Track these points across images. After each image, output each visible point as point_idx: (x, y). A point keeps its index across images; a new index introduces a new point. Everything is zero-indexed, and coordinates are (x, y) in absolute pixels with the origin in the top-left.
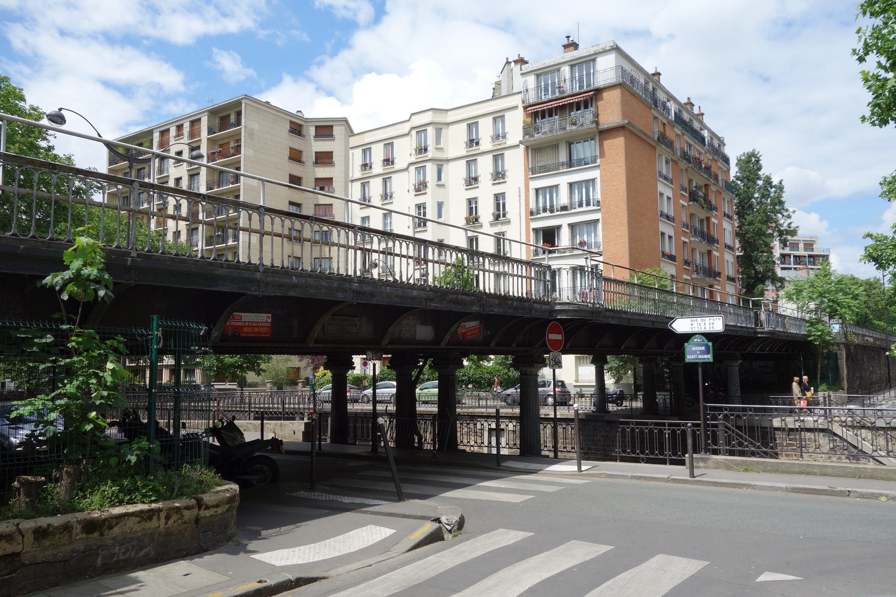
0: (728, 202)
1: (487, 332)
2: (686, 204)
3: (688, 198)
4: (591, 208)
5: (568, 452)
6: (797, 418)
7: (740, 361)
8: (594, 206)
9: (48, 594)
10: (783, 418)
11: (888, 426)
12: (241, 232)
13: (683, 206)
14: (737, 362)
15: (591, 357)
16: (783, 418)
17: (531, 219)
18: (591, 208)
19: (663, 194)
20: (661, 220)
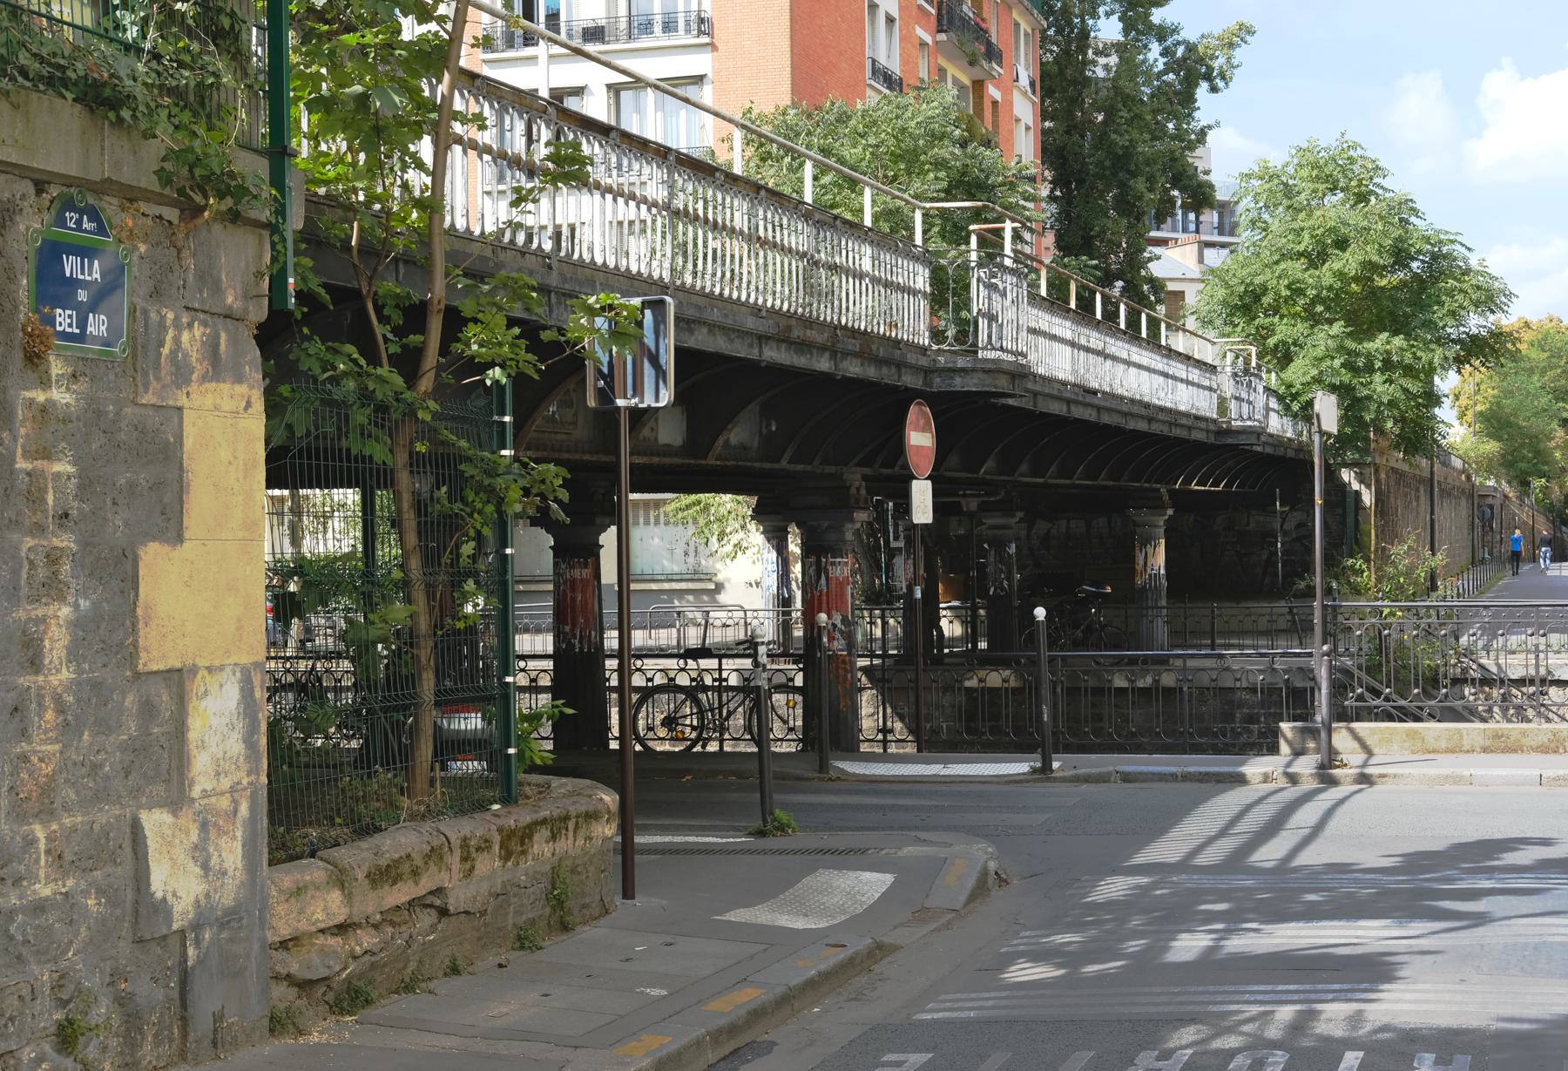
0: (1026, 34)
1: (768, 425)
2: (928, 39)
3: (933, 20)
4: (681, 38)
5: (660, 739)
6: (724, 684)
7: (1170, 512)
8: (688, 31)
9: (1246, 836)
10: (650, 684)
11: (1213, 684)
12: (458, 149)
13: (923, 44)
14: (1013, 516)
15: (754, 500)
16: (650, 684)
17: (484, 61)
18: (681, 38)
19: (877, 6)
20: (871, 86)
